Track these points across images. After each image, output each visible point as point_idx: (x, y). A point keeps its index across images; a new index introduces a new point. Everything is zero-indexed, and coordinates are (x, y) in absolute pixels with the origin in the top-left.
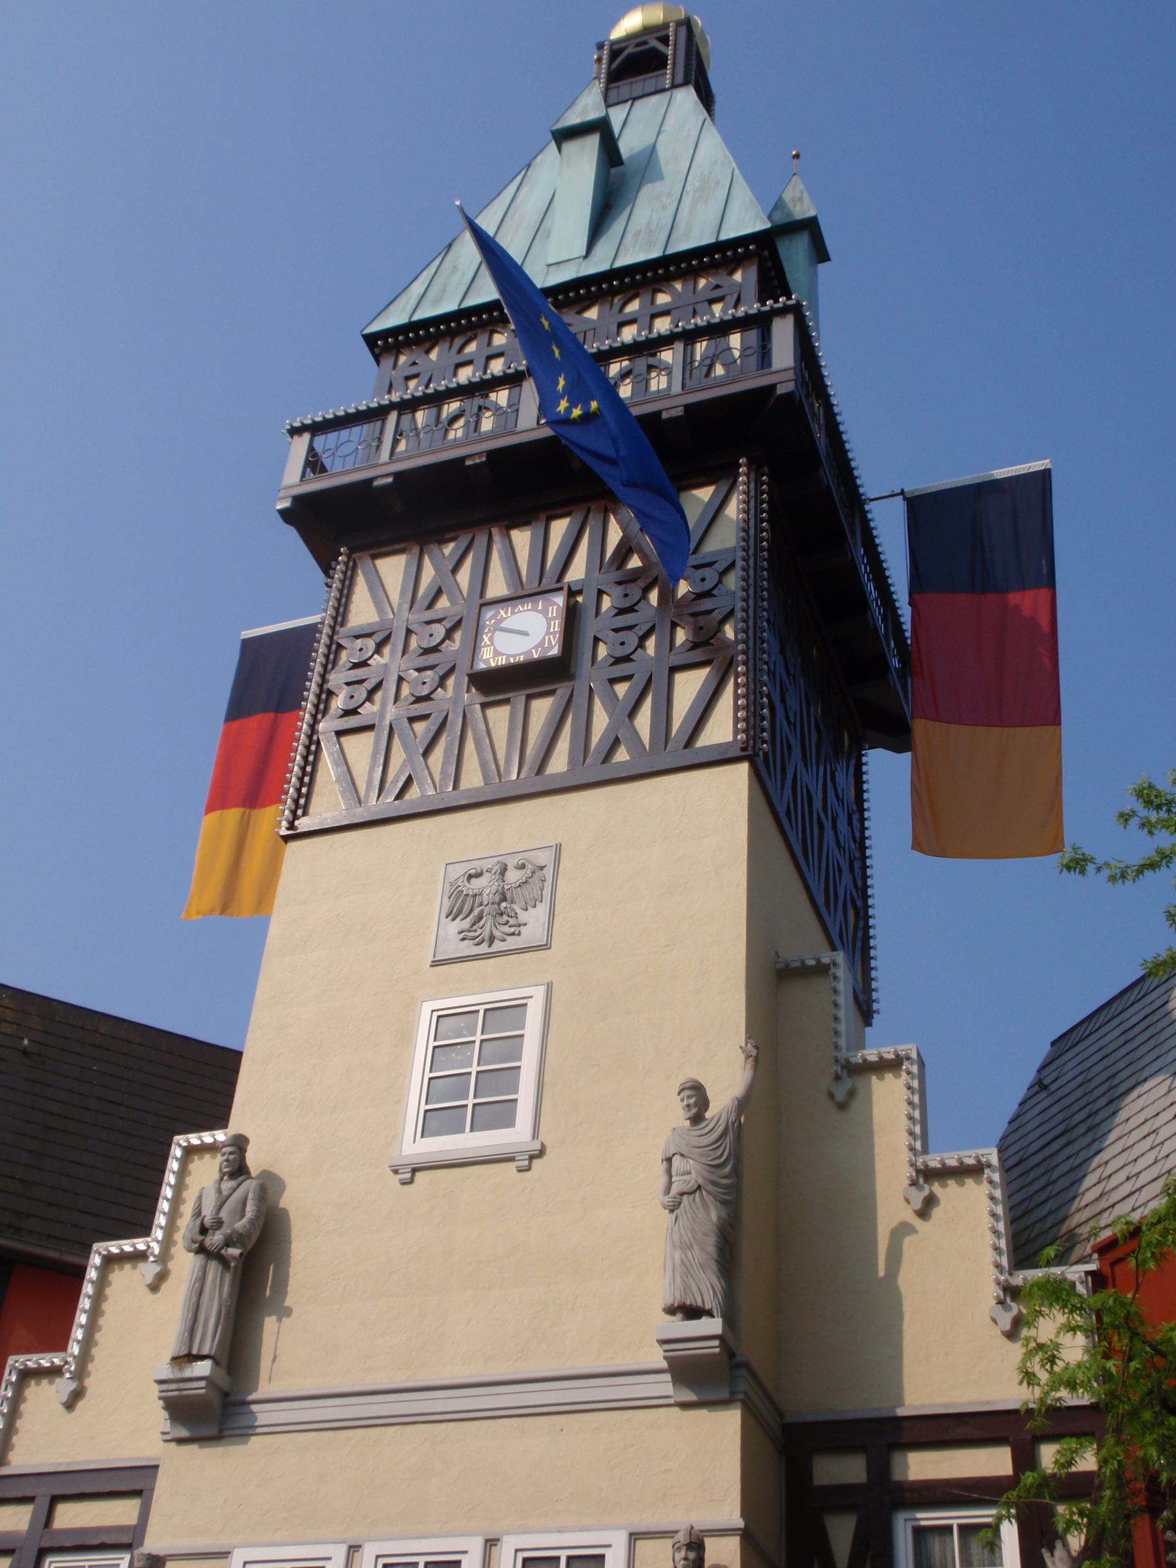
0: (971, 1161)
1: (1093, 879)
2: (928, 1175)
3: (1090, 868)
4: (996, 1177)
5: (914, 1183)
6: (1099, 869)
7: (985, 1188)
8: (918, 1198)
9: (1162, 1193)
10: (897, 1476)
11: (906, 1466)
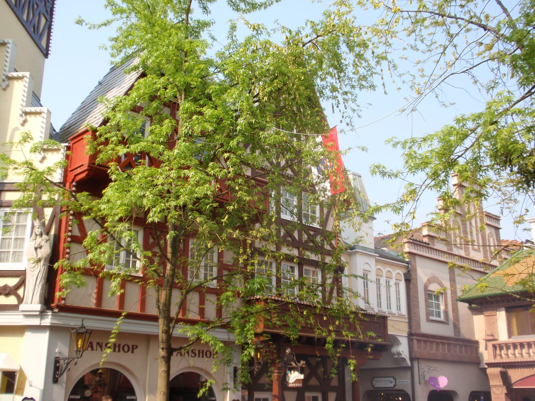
0: (21, 76)
1: (85, 27)
2: (26, 113)
3: (84, 24)
4: (27, 80)
5: (21, 116)
6: (86, 24)
7: (24, 83)
8: (22, 119)
9: (158, 291)
10: (2, 199)
11: (5, 196)
